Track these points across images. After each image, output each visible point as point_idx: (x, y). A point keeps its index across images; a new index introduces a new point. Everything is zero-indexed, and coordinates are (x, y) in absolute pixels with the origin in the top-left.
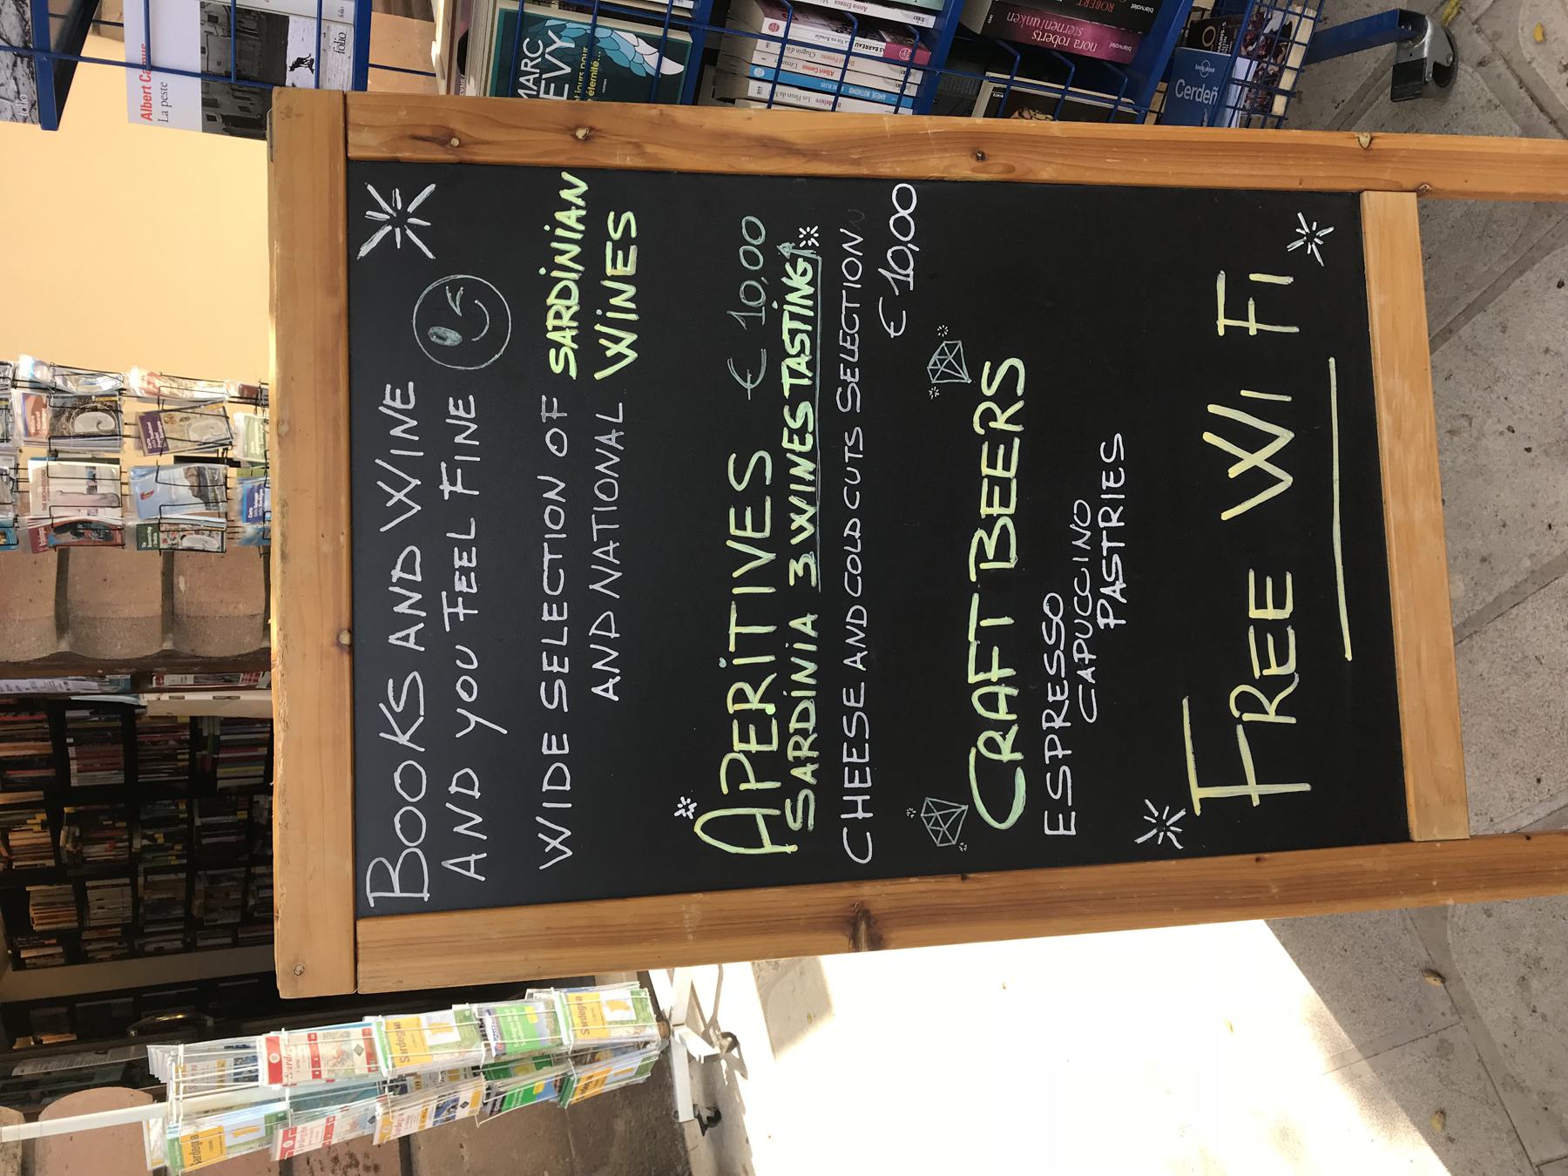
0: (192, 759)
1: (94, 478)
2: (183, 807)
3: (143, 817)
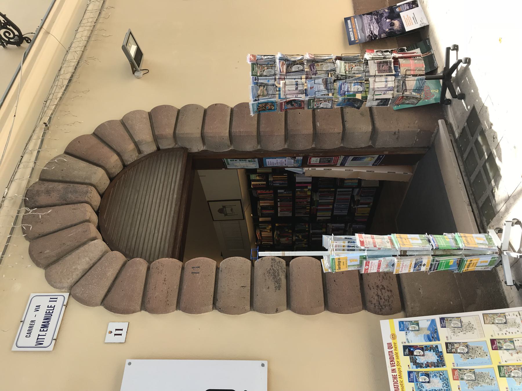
0: (310, 209)
1: (297, 85)
2: (307, 226)
3: (296, 229)
